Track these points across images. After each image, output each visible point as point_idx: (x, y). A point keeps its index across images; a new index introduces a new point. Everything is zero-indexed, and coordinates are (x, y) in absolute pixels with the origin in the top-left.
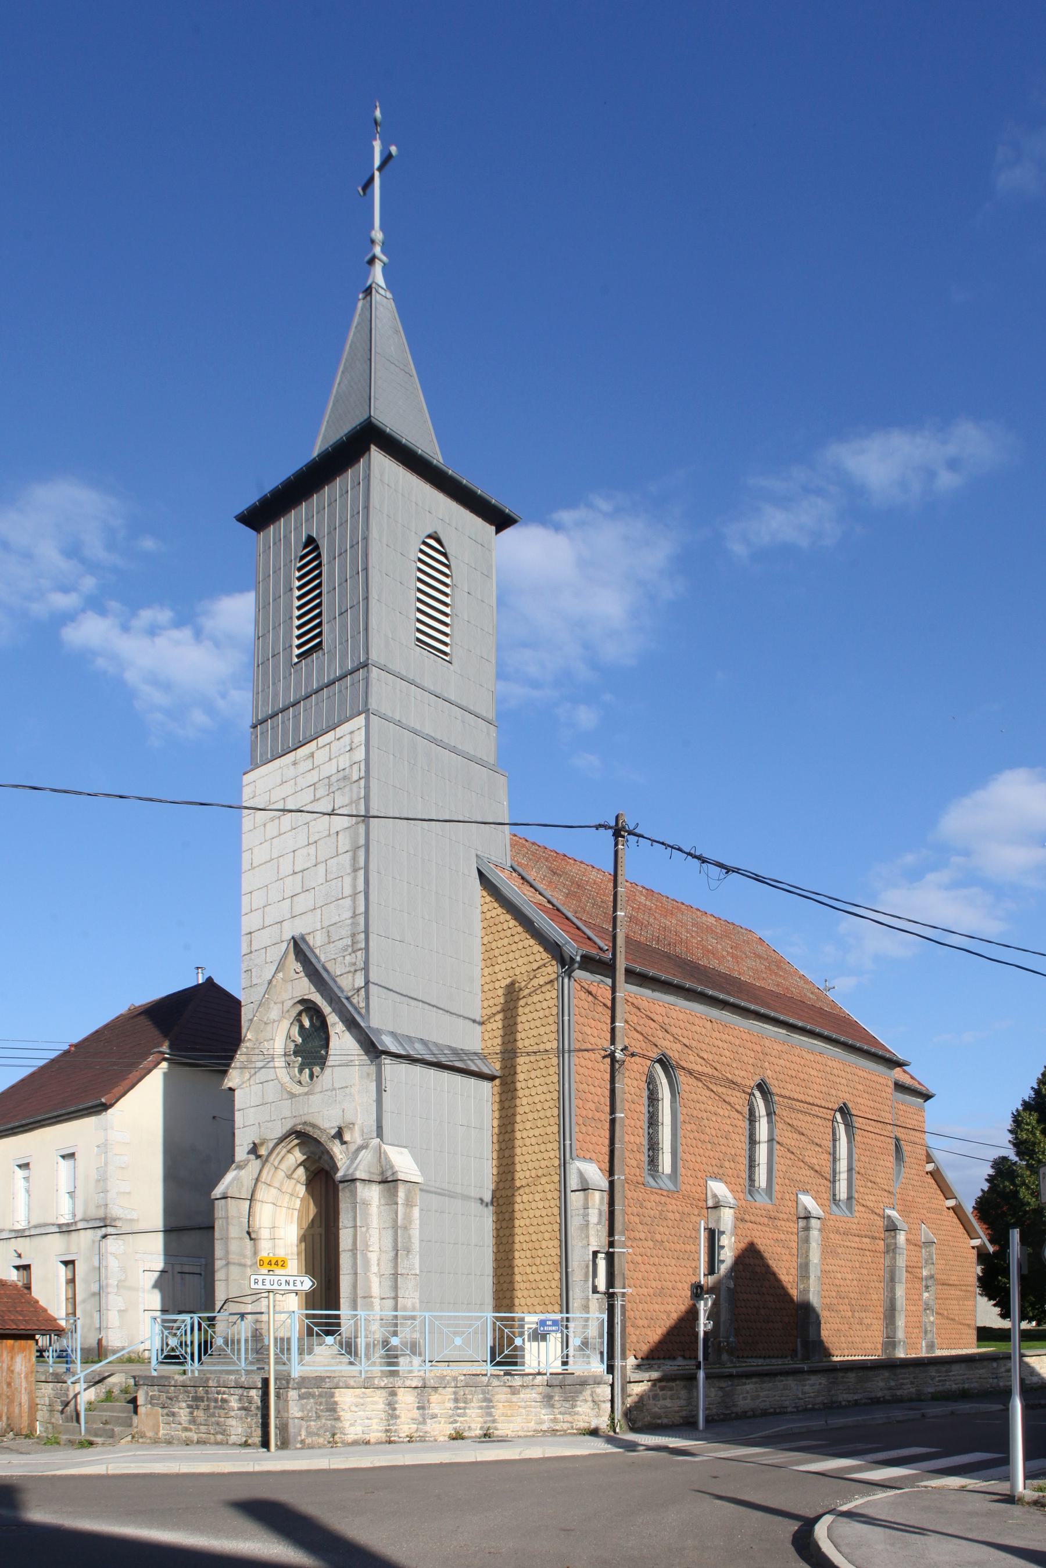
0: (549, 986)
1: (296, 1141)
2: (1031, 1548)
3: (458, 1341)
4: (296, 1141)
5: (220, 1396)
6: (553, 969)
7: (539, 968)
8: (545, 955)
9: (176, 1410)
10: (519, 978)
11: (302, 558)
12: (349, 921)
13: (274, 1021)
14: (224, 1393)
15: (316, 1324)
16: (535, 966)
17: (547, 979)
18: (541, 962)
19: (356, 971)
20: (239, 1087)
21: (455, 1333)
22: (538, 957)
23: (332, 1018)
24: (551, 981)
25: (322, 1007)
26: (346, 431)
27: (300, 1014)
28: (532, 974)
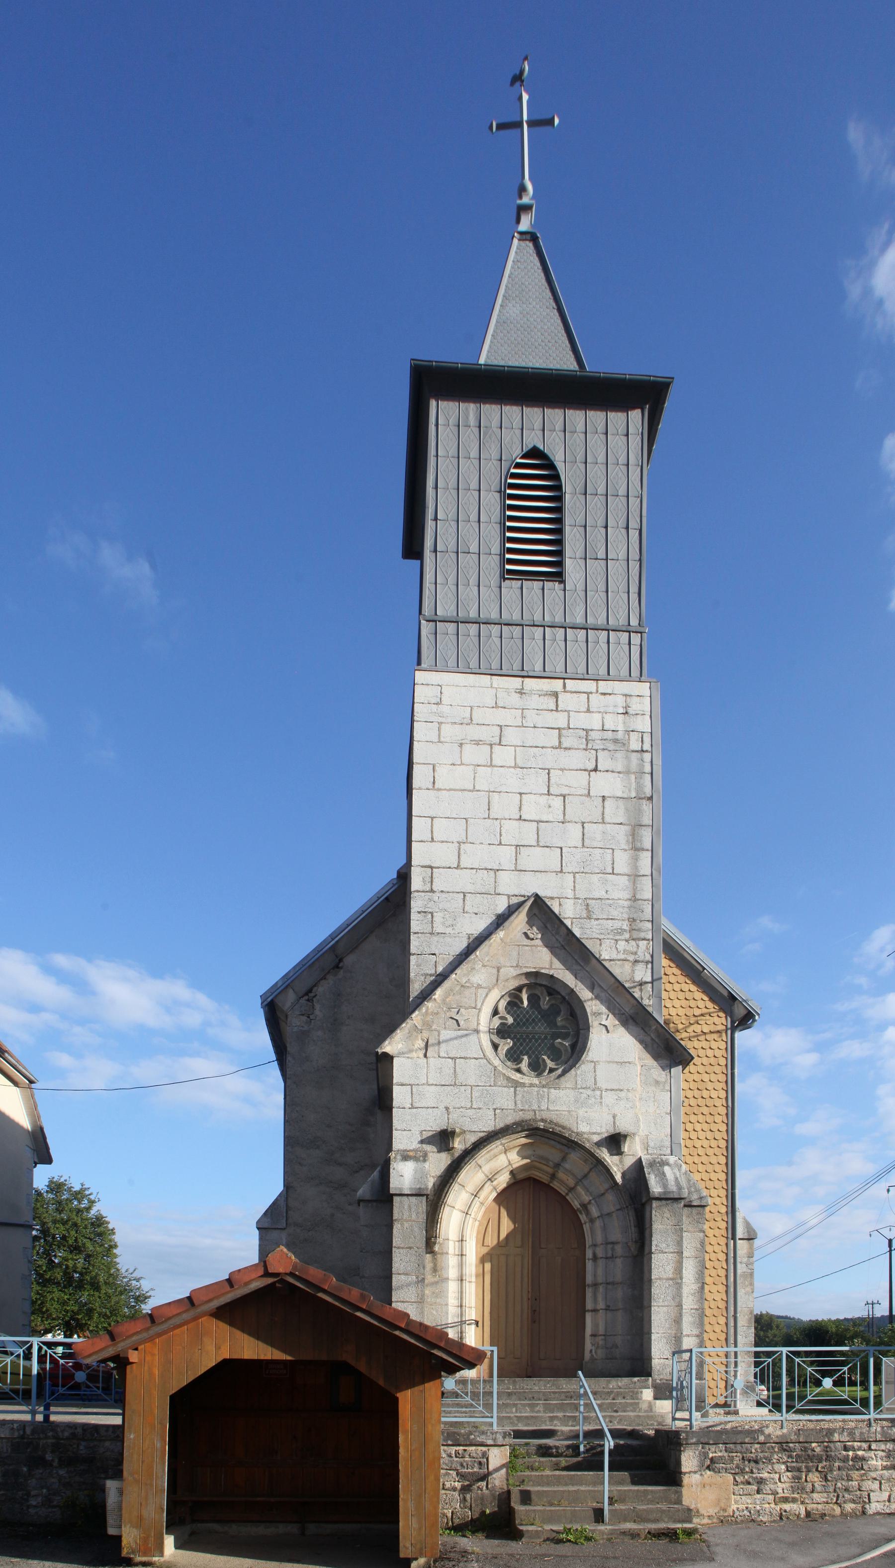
0: (715, 1036)
1: (524, 1141)
2: (264, 1562)
3: (828, 1383)
4: (524, 1141)
5: (851, 1453)
6: (720, 1021)
7: (702, 1015)
8: (710, 1005)
9: (765, 1475)
10: (675, 1019)
11: (518, 466)
12: (626, 903)
13: (479, 986)
14: (860, 1449)
15: (812, 1363)
16: (697, 1012)
17: (713, 1028)
18: (705, 1011)
19: (636, 961)
20: (401, 1054)
21: (825, 1374)
22: (701, 1004)
23: (593, 1006)
24: (718, 1032)
25: (577, 990)
26: (537, 365)
27: (519, 989)
28: (692, 1020)
